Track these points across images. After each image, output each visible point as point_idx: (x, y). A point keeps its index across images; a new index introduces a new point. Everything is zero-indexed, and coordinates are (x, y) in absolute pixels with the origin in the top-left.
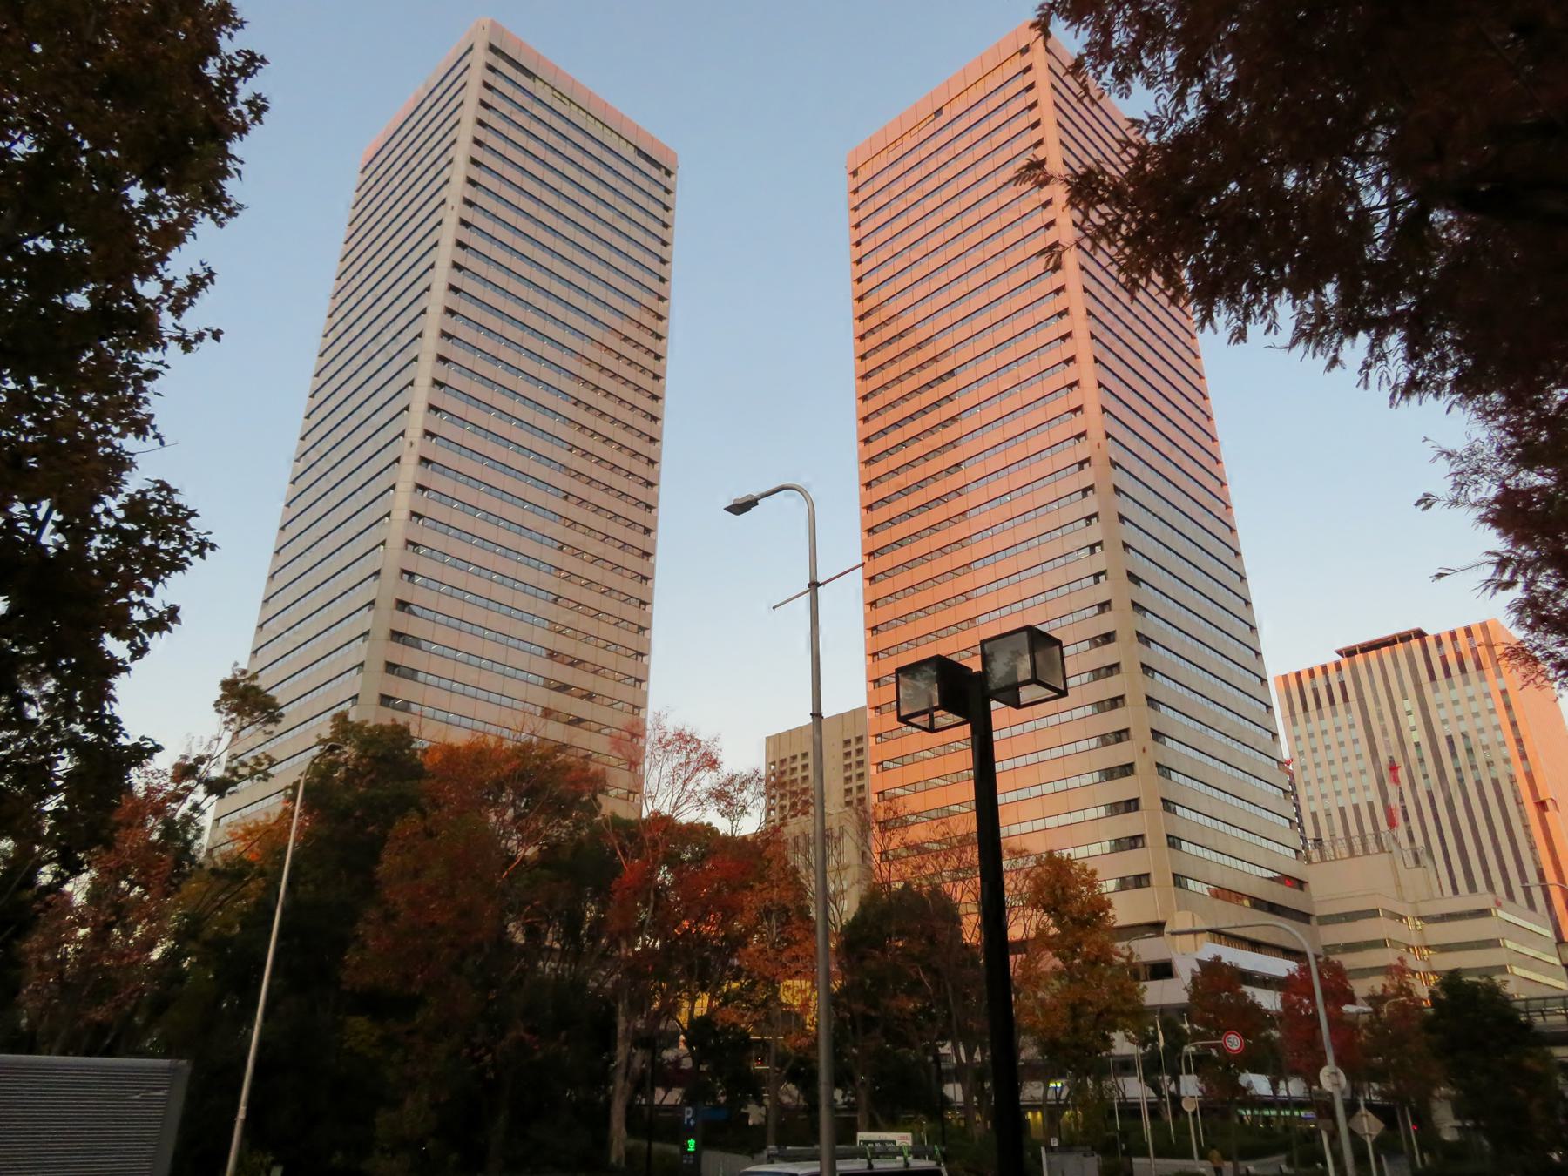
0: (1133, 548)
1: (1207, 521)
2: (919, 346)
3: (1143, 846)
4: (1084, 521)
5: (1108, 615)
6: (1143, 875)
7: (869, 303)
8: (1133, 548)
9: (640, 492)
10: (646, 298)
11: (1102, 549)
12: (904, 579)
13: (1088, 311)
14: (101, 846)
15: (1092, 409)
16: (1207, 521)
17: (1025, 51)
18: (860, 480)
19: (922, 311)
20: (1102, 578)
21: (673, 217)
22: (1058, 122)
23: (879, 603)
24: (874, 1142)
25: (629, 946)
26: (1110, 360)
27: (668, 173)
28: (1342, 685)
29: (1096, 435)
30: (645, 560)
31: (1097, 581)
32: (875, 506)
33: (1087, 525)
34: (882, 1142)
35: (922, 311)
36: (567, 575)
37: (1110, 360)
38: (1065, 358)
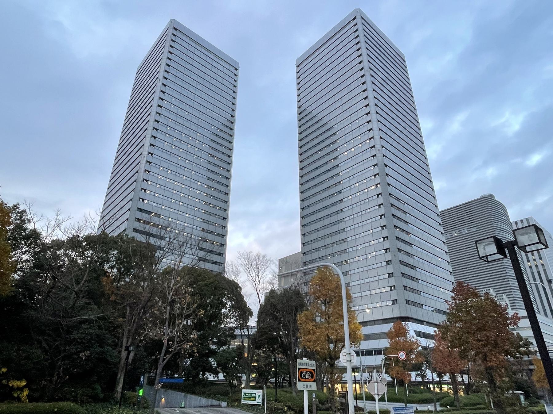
0: (388, 166)
1: (426, 203)
2: (317, 122)
3: (397, 304)
4: (384, 250)
5: (387, 241)
6: (391, 273)
7: (302, 109)
8: (388, 166)
9: (224, 181)
10: (220, 171)
11: (386, 228)
12: (313, 218)
13: (382, 146)
14: (115, 236)
15: (377, 137)
16: (426, 203)
17: (354, 19)
18: (300, 191)
19: (319, 109)
20: (383, 216)
21: (238, 72)
22: (372, 82)
23: (304, 208)
24: (248, 393)
25: (234, 337)
26: (377, 89)
27: (236, 69)
28: (465, 225)
29: (378, 146)
30: (227, 188)
31: (383, 229)
32: (303, 154)
33: (378, 197)
34: (251, 394)
35: (319, 109)
36: (213, 206)
37: (377, 89)
38: (365, 105)
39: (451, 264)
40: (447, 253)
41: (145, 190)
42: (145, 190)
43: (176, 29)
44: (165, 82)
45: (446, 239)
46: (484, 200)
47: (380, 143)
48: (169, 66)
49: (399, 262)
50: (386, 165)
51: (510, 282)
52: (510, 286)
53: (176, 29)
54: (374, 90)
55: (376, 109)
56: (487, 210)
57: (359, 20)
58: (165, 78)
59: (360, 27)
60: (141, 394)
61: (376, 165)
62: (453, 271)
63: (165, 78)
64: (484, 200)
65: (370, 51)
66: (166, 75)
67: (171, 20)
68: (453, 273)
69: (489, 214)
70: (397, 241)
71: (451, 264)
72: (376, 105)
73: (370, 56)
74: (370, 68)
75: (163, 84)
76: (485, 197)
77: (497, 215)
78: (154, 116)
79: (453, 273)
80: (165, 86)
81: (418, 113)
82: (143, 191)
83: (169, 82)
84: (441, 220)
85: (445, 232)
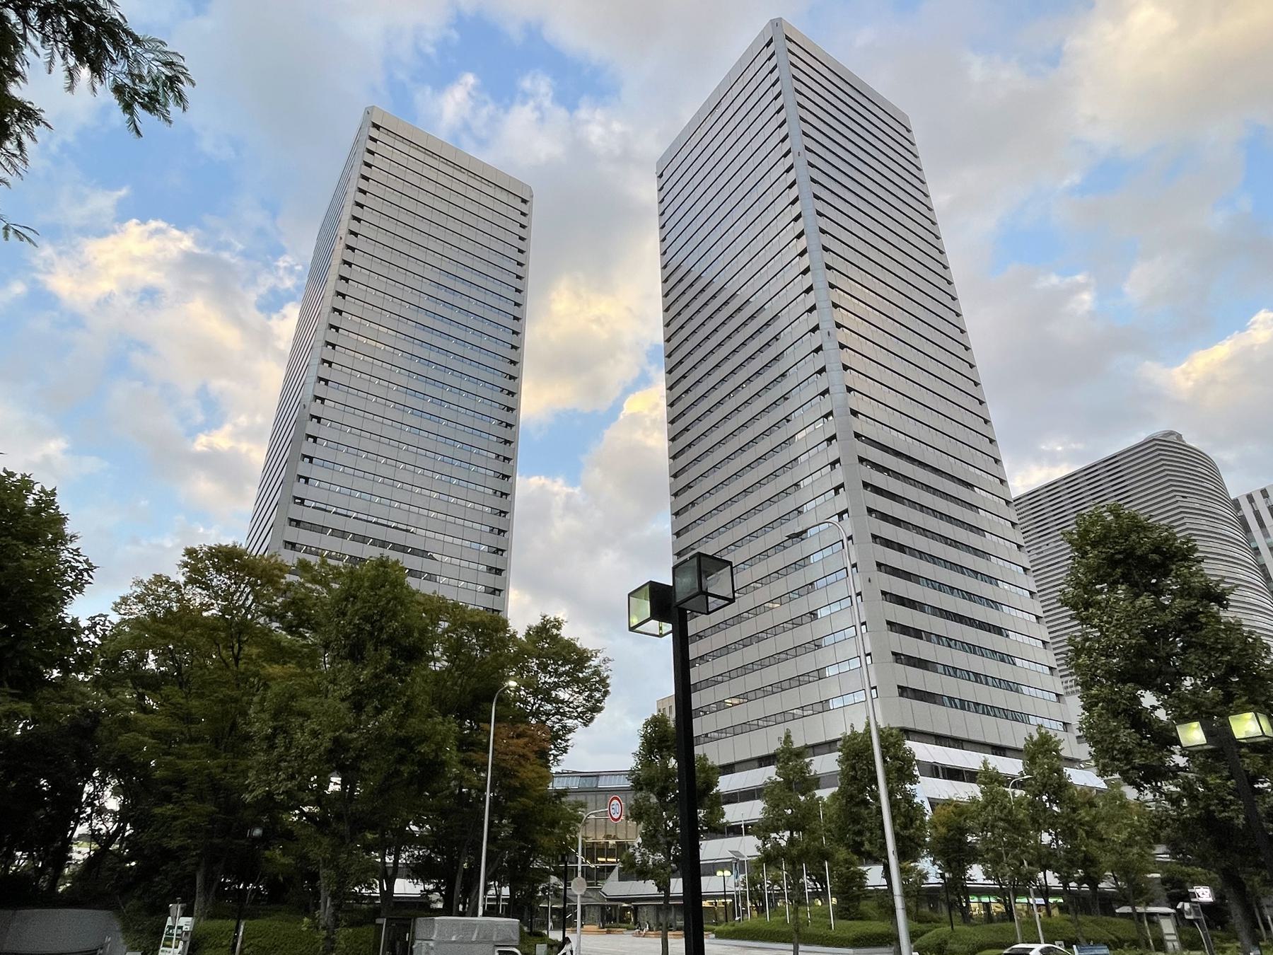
29: (827, 326)
39: (1040, 596)
40: (1047, 645)
41: (315, 439)
42: (307, 480)
43: (377, 127)
44: (352, 241)
45: (1031, 562)
46: (1168, 487)
47: (808, 172)
48: (362, 206)
49: (891, 657)
50: (855, 413)
51: (1177, 498)
52: (1187, 529)
53: (377, 127)
54: (813, 180)
55: (828, 276)
56: (1162, 469)
57: (779, 45)
58: (352, 233)
59: (782, 59)
60: (337, 586)
61: (831, 413)
62: (1058, 665)
63: (352, 233)
64: (1168, 487)
65: (813, 139)
66: (355, 226)
67: (366, 109)
68: (1053, 643)
69: (1162, 469)
70: (863, 467)
71: (1040, 596)
72: (829, 267)
73: (798, 68)
74: (807, 148)
75: (348, 247)
76: (1154, 439)
77: (1189, 478)
78: (326, 316)
79: (1053, 643)
80: (353, 249)
81: (927, 175)
82: (303, 480)
83: (376, 172)
84: (1035, 584)
85: (1040, 589)
